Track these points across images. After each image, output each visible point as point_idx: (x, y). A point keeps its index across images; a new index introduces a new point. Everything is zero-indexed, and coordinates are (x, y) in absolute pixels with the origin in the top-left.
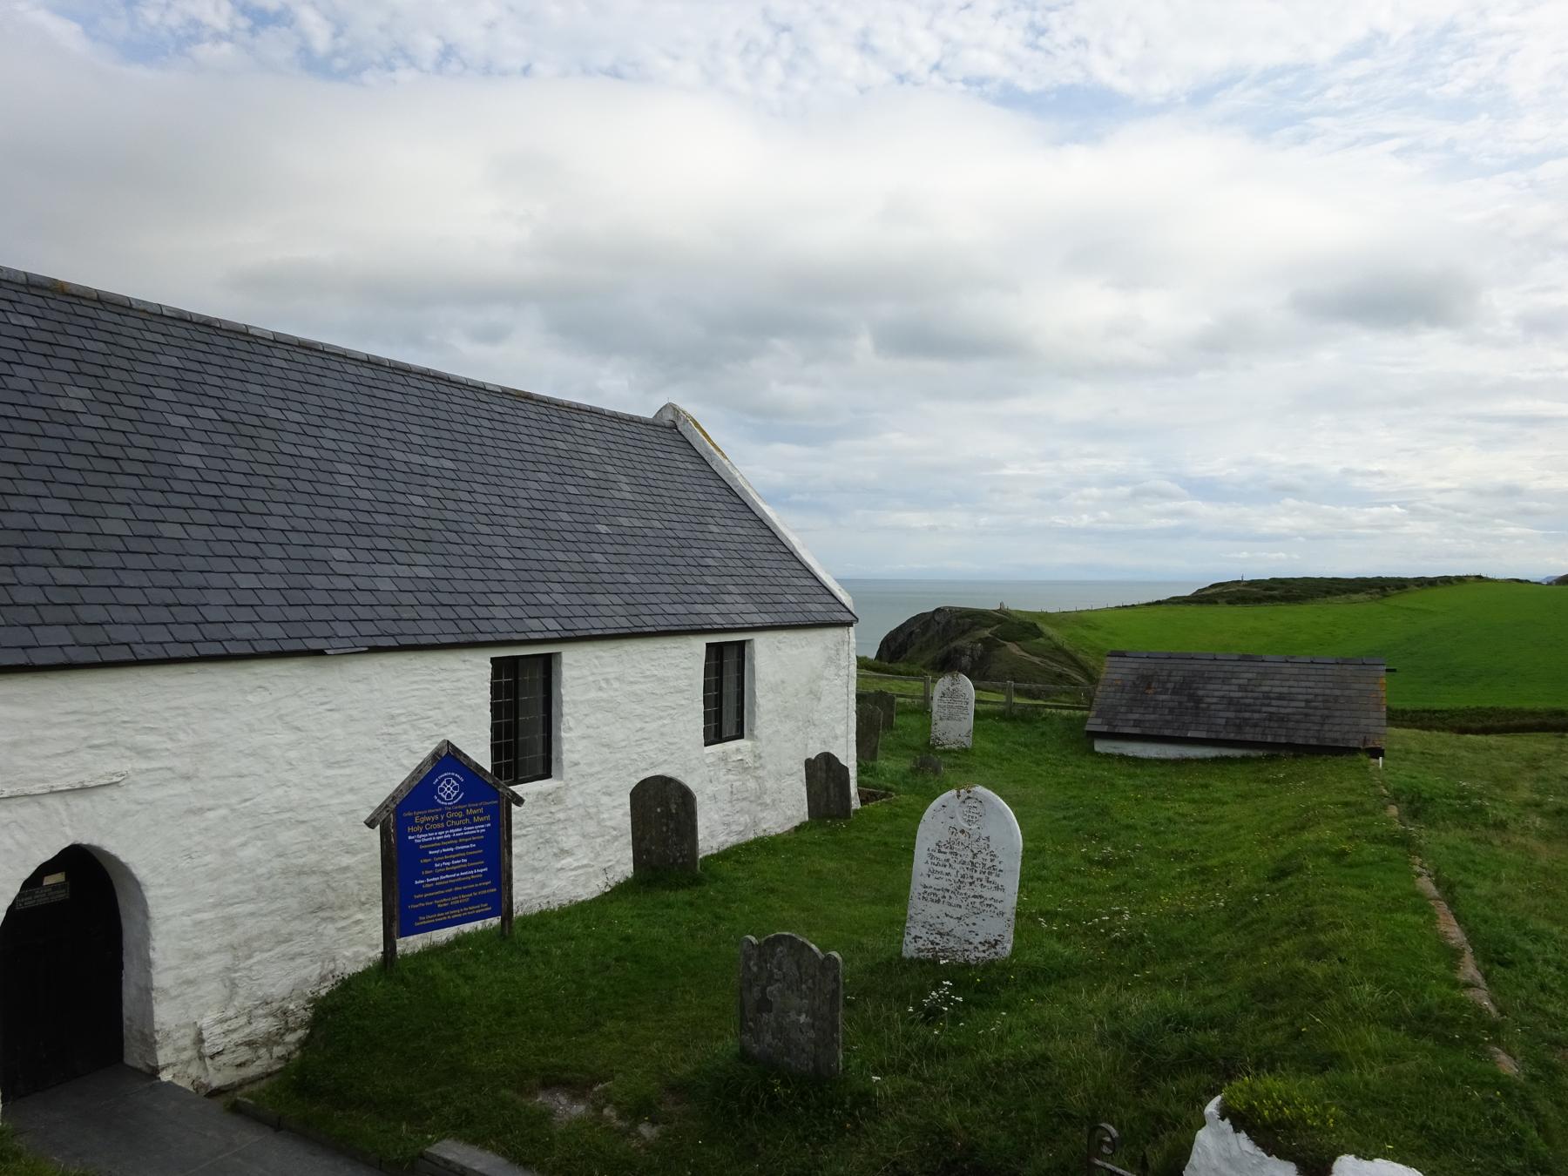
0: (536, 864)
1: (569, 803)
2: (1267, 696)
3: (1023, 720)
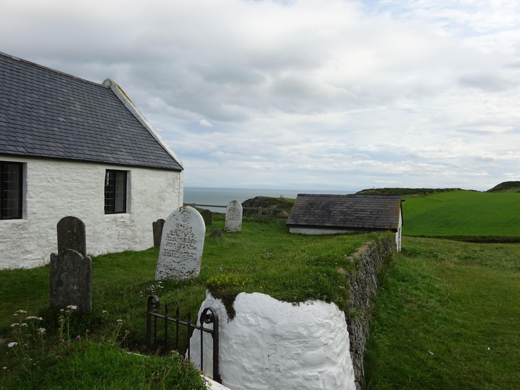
0: (11, 255)
1: (30, 230)
2: (356, 210)
3: (265, 223)
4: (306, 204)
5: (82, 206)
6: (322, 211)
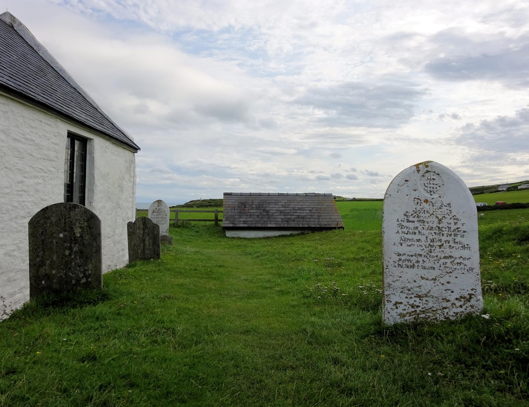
2: (294, 209)
3: (184, 227)
4: (236, 204)
5: (37, 191)
6: (258, 211)
